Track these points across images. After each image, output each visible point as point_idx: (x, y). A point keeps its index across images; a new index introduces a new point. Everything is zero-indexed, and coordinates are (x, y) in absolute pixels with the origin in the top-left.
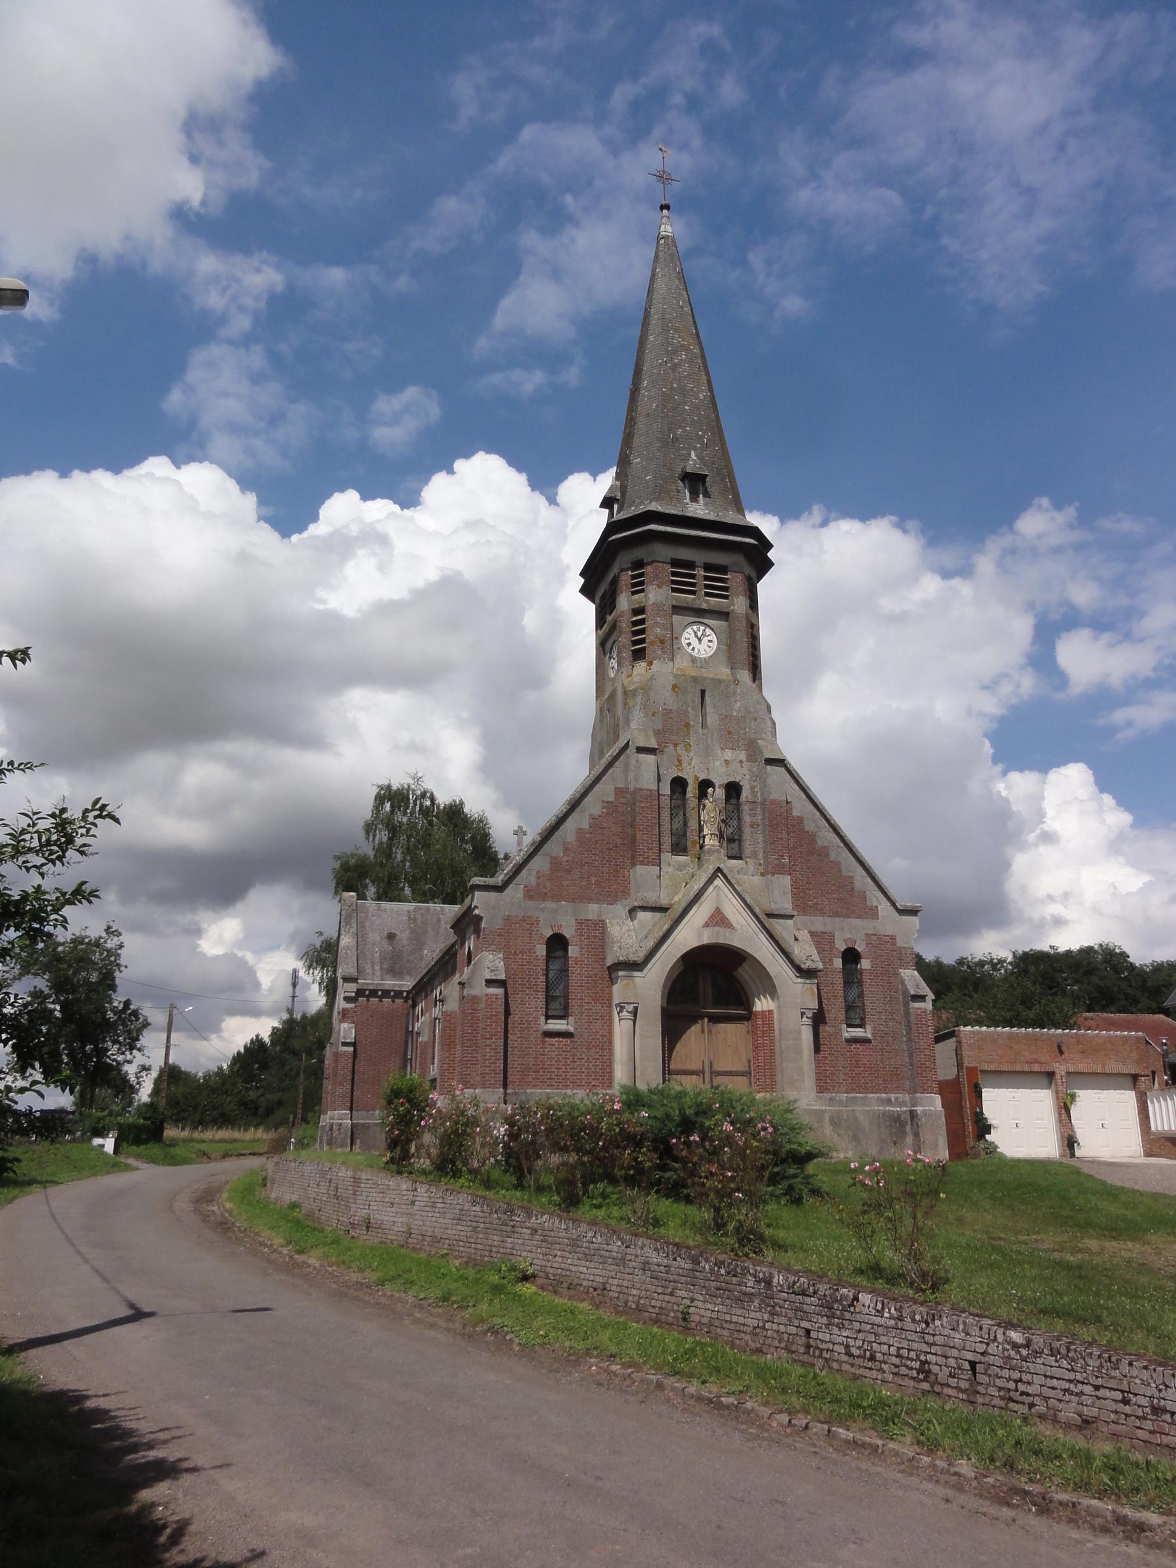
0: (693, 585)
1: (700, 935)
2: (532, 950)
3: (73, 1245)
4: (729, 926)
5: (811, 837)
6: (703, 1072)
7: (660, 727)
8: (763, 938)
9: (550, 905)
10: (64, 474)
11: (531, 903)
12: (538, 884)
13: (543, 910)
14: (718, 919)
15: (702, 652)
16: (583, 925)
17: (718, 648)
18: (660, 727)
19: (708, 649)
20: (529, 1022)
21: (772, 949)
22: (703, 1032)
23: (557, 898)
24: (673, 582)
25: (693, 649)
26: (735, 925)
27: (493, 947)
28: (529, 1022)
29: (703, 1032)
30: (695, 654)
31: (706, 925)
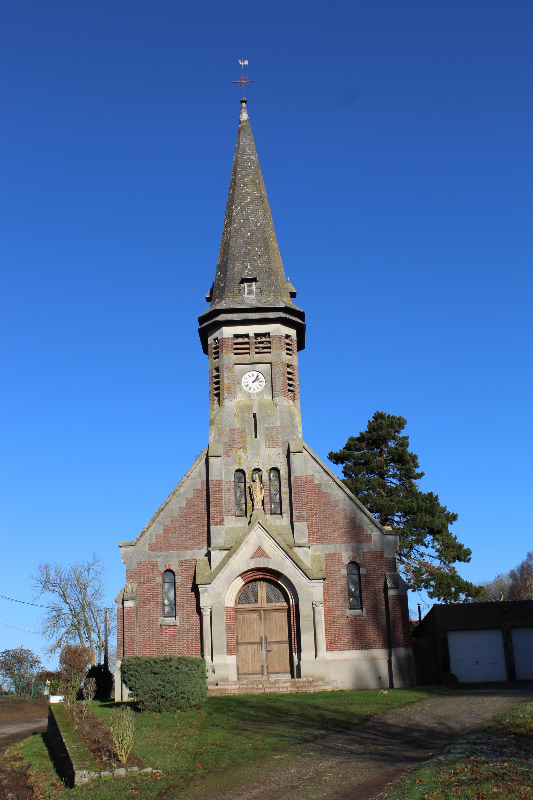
0: (248, 349)
1: (248, 564)
2: (154, 580)
3: (140, 537)
4: (267, 557)
5: (326, 495)
6: (261, 643)
7: (227, 440)
8: (288, 561)
9: (164, 553)
10: (56, 772)
11: (153, 554)
12: (157, 542)
13: (160, 556)
14: (260, 553)
15: (256, 389)
16: (183, 563)
17: (266, 386)
18: (227, 440)
19: (259, 387)
20: (153, 621)
21: (294, 568)
22: (260, 619)
23: (167, 549)
24: (235, 349)
25: (250, 388)
26: (270, 556)
27: (132, 580)
28: (153, 621)
29: (260, 619)
30: (251, 391)
31: (252, 557)
